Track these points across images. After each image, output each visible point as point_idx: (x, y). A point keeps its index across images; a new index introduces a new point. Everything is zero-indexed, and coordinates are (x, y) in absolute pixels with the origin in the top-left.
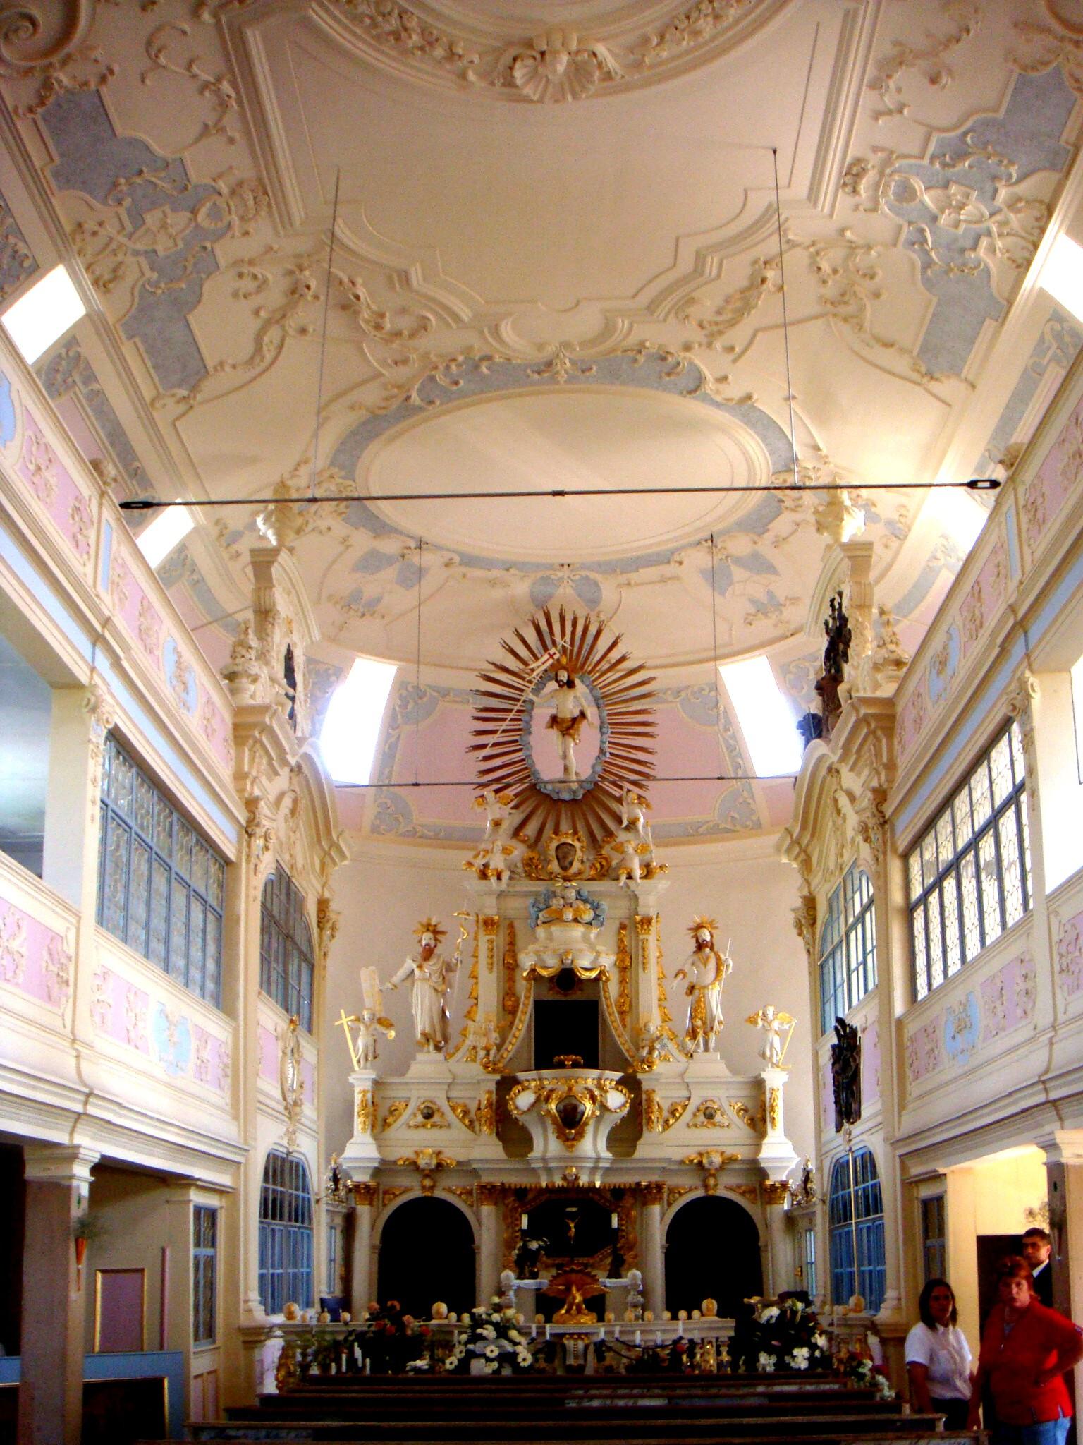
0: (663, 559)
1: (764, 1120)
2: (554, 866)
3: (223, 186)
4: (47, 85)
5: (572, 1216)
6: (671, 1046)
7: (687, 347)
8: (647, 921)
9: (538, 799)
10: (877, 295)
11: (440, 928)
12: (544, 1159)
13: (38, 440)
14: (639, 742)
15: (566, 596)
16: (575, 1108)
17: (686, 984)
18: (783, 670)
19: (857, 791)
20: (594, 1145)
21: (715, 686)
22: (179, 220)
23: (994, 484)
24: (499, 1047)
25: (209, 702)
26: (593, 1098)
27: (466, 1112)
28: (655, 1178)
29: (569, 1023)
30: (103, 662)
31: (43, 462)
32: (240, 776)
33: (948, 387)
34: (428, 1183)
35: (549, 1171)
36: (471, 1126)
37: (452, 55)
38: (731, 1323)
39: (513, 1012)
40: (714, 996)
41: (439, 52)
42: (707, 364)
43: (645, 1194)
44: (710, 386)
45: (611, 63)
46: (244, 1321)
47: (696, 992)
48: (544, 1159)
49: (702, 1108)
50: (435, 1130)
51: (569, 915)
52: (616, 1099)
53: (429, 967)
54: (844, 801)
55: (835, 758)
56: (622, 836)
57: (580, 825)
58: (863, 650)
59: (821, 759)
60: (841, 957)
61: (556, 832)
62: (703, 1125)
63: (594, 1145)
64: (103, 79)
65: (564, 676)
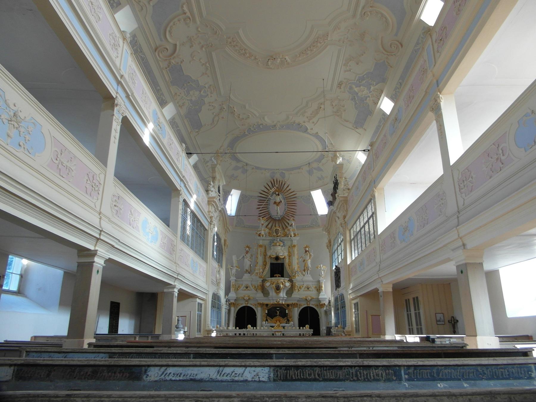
0: (299, 168)
2: (275, 234)
3: (207, 86)
4: (170, 63)
5: (278, 310)
6: (300, 273)
7: (304, 122)
8: (294, 246)
9: (271, 219)
10: (345, 111)
13: (170, 138)
14: (293, 207)
15: (278, 176)
18: (324, 193)
19: (340, 216)
20: (283, 294)
21: (310, 196)
22: (197, 93)
23: (369, 150)
25: (203, 196)
26: (283, 284)
28: (296, 302)
29: (278, 268)
30: (182, 185)
31: (171, 143)
32: (209, 212)
33: (360, 130)
35: (273, 300)
36: (256, 290)
37: (255, 59)
38: (312, 330)
39: (265, 265)
41: (253, 58)
42: (309, 126)
43: (295, 305)
44: (309, 131)
45: (289, 61)
46: (207, 328)
51: (278, 244)
52: (288, 284)
53: (249, 255)
54: (337, 219)
55: (335, 210)
56: (289, 227)
57: (280, 225)
58: (341, 186)
59: (332, 210)
60: (336, 253)
63: (283, 294)
64: (182, 62)
65: (277, 193)
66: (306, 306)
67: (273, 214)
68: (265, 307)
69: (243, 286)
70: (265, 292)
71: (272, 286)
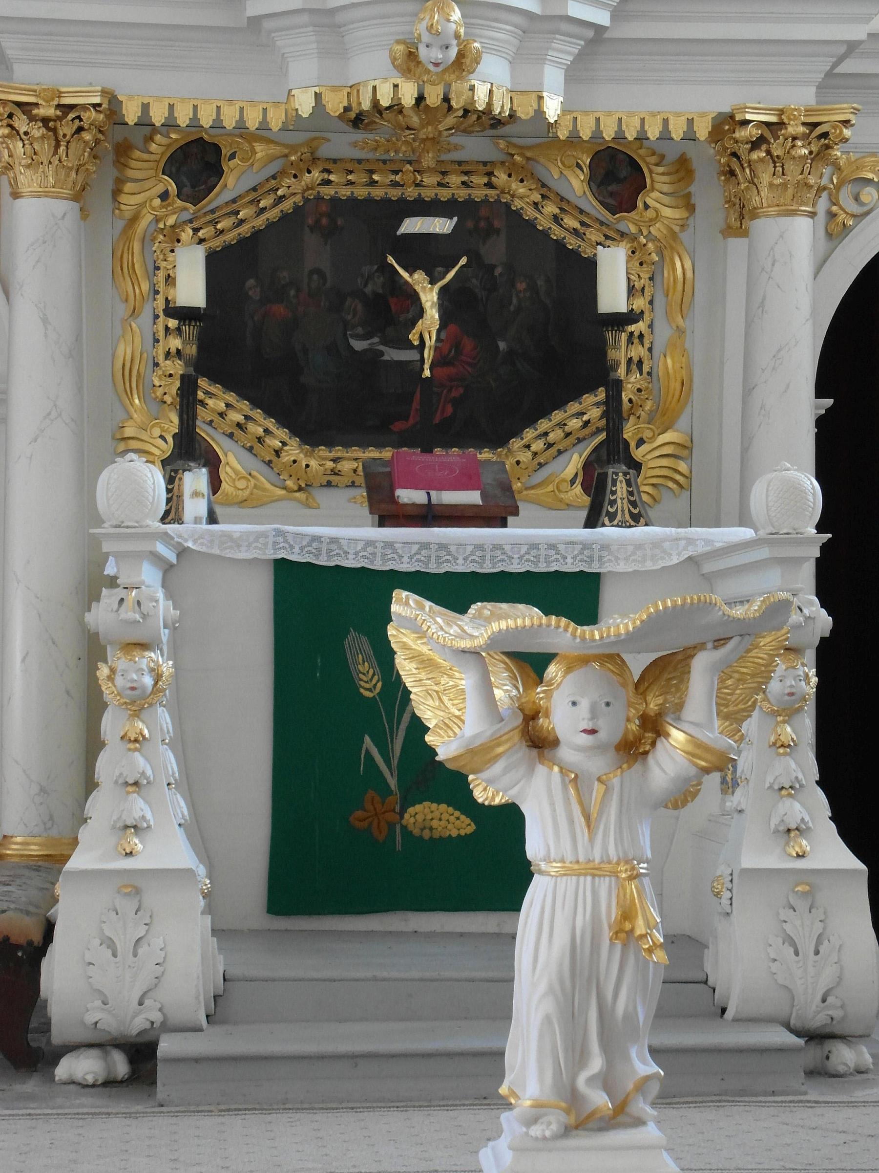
5: (426, 254)
28: (800, 97)
68: (148, 190)
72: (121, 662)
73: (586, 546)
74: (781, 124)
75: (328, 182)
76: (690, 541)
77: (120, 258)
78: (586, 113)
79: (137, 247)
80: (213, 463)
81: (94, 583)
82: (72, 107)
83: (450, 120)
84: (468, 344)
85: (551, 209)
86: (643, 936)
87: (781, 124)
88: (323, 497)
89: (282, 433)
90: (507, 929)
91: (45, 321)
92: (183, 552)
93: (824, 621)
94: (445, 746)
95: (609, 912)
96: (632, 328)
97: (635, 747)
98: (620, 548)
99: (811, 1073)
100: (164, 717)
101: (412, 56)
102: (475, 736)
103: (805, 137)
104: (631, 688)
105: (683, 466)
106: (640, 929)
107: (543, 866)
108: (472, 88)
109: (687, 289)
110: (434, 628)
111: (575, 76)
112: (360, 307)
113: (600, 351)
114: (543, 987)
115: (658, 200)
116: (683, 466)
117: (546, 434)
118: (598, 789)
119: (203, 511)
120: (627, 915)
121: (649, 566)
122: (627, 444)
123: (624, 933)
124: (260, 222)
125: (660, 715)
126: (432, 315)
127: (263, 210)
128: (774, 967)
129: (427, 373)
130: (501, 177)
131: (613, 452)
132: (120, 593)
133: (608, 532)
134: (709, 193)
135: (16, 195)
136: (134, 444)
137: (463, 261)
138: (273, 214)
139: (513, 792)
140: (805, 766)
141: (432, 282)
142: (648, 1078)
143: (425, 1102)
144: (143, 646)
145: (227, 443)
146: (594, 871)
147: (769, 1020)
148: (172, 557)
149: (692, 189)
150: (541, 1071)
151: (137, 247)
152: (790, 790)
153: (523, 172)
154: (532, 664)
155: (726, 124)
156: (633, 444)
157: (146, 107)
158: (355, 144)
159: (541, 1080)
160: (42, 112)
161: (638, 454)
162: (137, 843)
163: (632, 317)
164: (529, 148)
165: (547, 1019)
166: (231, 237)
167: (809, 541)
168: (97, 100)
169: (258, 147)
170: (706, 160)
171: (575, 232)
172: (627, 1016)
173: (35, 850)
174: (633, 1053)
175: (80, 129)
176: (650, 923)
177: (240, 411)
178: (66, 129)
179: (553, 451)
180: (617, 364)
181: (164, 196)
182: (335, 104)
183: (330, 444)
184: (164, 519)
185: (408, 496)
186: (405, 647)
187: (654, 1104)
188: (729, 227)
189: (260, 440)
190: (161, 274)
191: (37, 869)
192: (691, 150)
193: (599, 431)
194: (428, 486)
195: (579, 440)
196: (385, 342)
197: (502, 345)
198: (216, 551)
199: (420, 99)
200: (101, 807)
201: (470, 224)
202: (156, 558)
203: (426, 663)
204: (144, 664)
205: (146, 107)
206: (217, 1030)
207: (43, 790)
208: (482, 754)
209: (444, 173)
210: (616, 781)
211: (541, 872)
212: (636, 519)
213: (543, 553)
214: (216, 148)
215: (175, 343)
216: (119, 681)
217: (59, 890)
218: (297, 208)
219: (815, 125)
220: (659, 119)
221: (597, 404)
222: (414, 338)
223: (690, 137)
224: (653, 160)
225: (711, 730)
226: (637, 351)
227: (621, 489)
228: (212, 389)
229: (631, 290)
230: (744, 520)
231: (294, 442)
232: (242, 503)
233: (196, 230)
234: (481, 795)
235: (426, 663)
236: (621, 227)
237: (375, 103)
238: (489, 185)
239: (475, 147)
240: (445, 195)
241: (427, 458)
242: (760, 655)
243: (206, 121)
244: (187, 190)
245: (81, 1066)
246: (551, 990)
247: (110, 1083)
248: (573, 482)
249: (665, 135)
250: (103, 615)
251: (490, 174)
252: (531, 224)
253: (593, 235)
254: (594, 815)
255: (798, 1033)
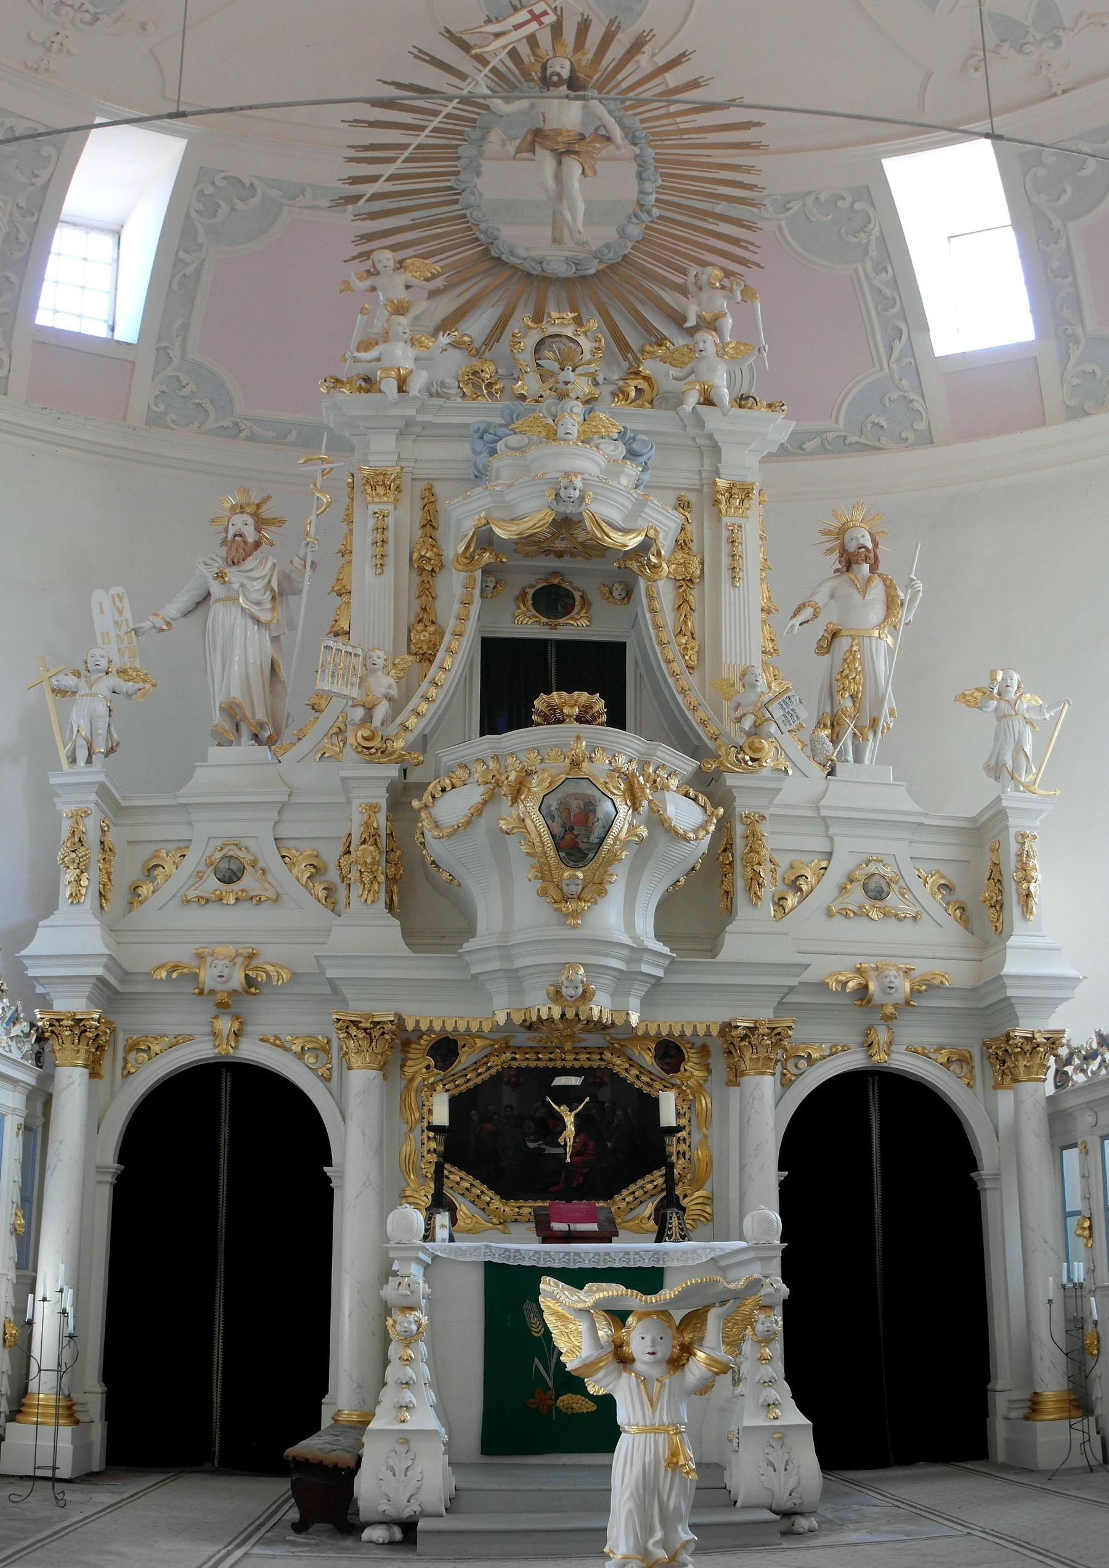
1: (998, 906)
5: (567, 1096)
8: (741, 492)
11: (267, 512)
12: (505, 950)
16: (589, 808)
17: (818, 629)
20: (625, 915)
24: (397, 704)
26: (633, 797)
27: (317, 870)
28: (765, 1014)
29: (554, 654)
34: (225, 1025)
35: (515, 978)
40: (882, 652)
43: (734, 1048)
47: (843, 644)
48: (505, 950)
49: (860, 875)
50: (247, 911)
53: (255, 577)
61: (538, 318)
62: (861, 913)
63: (625, 915)
66: (852, 1061)
67: (525, 240)
68: (419, 1064)
69: (194, 858)
70: (408, 880)
71: (506, 816)
72: (399, 1318)
73: (655, 1253)
74: (756, 1028)
75: (514, 1059)
76: (713, 1249)
77: (405, 1100)
78: (653, 1022)
79: (413, 1094)
80: (453, 1210)
81: (387, 1273)
82: (379, 1023)
83: (580, 1026)
84: (591, 1144)
85: (634, 1072)
86: (684, 1465)
87: (756, 1028)
88: (513, 1228)
89: (491, 1193)
90: (606, 1462)
91: (364, 1134)
92: (435, 1258)
93: (785, 1291)
94: (571, 1363)
95: (664, 1453)
96: (679, 1135)
97: (677, 1362)
98: (676, 1254)
99: (784, 1534)
100: (423, 1347)
101: (558, 992)
102: (587, 1358)
103: (769, 1035)
104: (675, 1329)
105: (708, 1209)
106: (682, 1461)
107: (627, 1428)
108: (591, 1009)
109: (708, 1114)
110: (563, 1297)
111: (646, 1003)
112: (532, 1125)
113: (662, 1147)
114: (627, 1494)
115: (691, 1066)
116: (708, 1209)
117: (634, 1193)
118: (657, 1385)
119: (447, 1236)
120: (674, 1454)
121: (690, 1263)
122: (678, 1197)
123: (673, 1464)
124: (478, 1080)
125: (691, 1344)
126: (571, 1128)
127: (480, 1074)
128: (762, 1478)
129: (568, 1160)
130: (607, 1055)
131: (670, 1202)
132: (399, 1279)
133: (667, 1245)
134: (719, 1063)
135: (350, 1068)
136: (411, 1200)
137: (587, 1099)
138: (486, 1076)
139: (609, 1387)
140: (778, 1369)
141: (571, 1111)
142: (688, 1542)
143: (568, 1556)
144: (412, 1309)
145: (460, 1198)
146: (655, 1430)
147: (760, 1507)
148: (429, 1261)
149: (710, 1061)
150: (627, 1541)
151: (413, 1094)
152: (770, 1383)
153: (620, 1053)
154: (619, 1317)
155: (727, 1028)
156: (681, 1198)
157: (418, 1022)
158: (529, 1039)
159: (627, 1545)
160: (363, 1025)
161: (684, 1202)
162: (407, 1415)
163: (679, 1129)
164: (623, 1040)
165: (630, 1511)
166: (463, 1088)
167: (775, 1247)
168: (392, 1019)
169: (477, 1041)
170: (717, 1047)
171: (648, 1084)
172: (675, 1508)
173: (354, 1418)
174: (680, 1529)
175: (383, 1033)
176: (688, 1457)
177: (467, 1181)
178: (376, 1033)
179: (638, 1201)
180: (672, 1154)
181: (428, 1067)
182: (518, 1019)
183: (517, 1199)
184: (425, 1238)
185: (558, 1226)
186: (549, 1308)
187: (692, 1554)
188: (730, 1081)
189: (478, 1197)
190: (426, 1109)
191: (355, 1428)
192: (708, 1041)
193: (662, 1190)
194: (569, 1221)
195: (652, 1196)
196: (545, 1144)
197: (609, 1145)
198: (453, 1257)
199: (563, 1015)
200: (388, 1396)
201: (592, 1080)
202: (419, 1261)
203: (560, 1317)
204: (411, 1318)
205: (418, 1022)
206: (450, 1516)
207: (359, 1386)
208: (592, 1366)
209: (577, 1054)
210: (667, 1381)
211: (625, 1432)
212: (683, 1238)
213: (632, 1257)
214: (456, 1042)
215: (433, 1145)
216: (398, 1327)
217: (365, 1439)
218: (498, 1072)
219: (774, 1028)
220: (691, 1025)
221: (661, 1176)
222: (561, 1141)
223: (708, 1034)
224: (689, 1046)
225: (720, 1351)
226: (683, 1147)
227: (675, 1221)
228: (453, 1170)
229: (678, 1115)
230: (741, 1238)
231: (497, 1198)
232: (469, 1231)
233: (444, 1085)
234: (591, 1390)
235: (560, 1317)
236: (673, 1081)
237: (539, 1017)
238: (601, 1059)
239: (594, 1040)
240: (577, 1065)
241: (569, 1205)
242: (746, 1310)
243: (449, 1028)
244: (440, 1064)
245: (376, 1534)
246: (632, 1496)
247: (392, 1543)
248: (649, 1218)
249: (695, 1034)
250: (390, 1291)
251: (601, 1054)
252: (624, 1080)
253: (657, 1085)
254: (655, 1399)
255: (776, 1513)
